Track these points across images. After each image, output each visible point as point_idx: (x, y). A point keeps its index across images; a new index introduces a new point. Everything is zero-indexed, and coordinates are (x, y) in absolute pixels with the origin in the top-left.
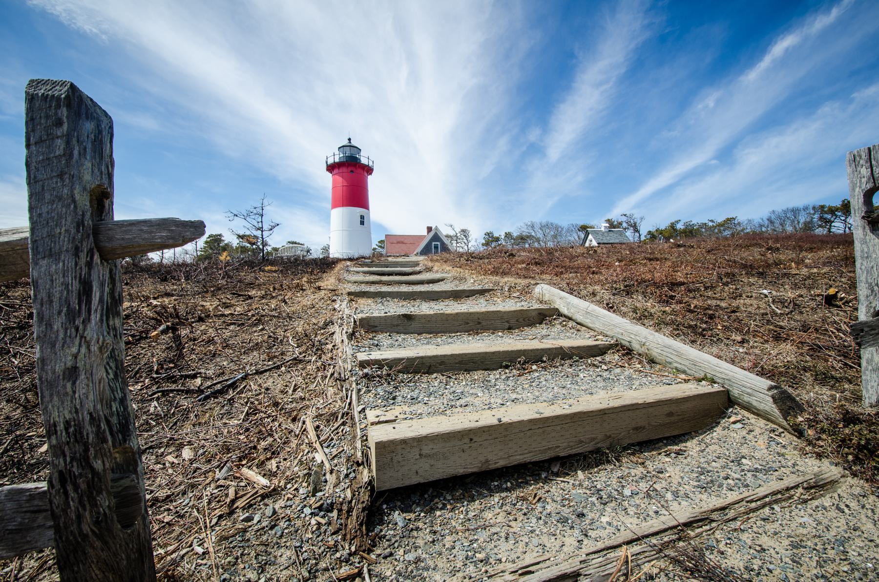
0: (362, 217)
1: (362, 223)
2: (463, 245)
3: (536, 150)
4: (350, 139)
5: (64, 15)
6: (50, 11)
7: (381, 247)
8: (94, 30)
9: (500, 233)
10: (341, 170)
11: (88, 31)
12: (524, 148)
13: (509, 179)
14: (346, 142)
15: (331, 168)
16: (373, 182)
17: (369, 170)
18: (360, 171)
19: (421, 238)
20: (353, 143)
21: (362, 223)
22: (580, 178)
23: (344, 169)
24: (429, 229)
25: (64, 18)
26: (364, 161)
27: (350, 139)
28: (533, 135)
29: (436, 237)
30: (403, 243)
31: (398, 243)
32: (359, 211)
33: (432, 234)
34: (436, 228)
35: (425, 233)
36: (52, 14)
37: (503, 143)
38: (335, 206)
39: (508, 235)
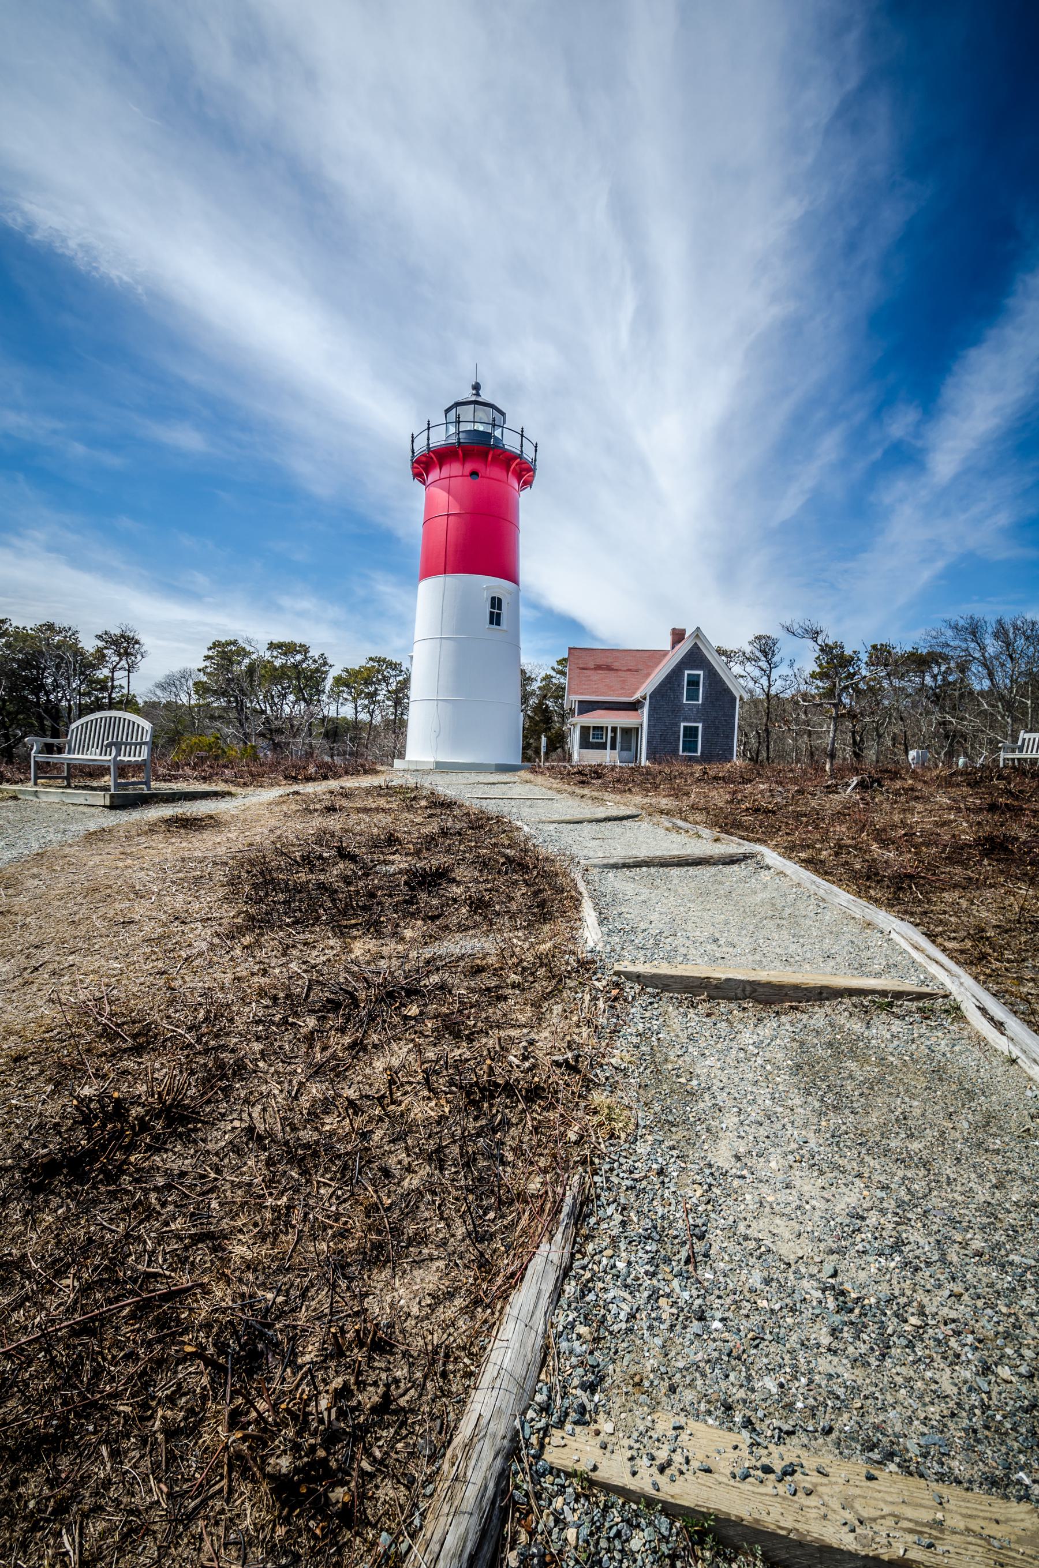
0: (496, 603)
1: (495, 619)
2: (757, 673)
3: (906, 457)
4: (477, 387)
5: (80, 255)
6: (60, 251)
7: (562, 673)
8: (126, 278)
9: (856, 638)
10: (446, 471)
11: (116, 281)
12: (877, 454)
13: (841, 526)
14: (468, 394)
15: (425, 464)
16: (533, 513)
17: (523, 471)
18: (496, 472)
19: (656, 656)
20: (485, 396)
21: (495, 619)
22: (1003, 518)
23: (455, 469)
24: (678, 636)
25: (81, 262)
26: (511, 442)
27: (477, 387)
28: (900, 424)
29: (695, 658)
30: (609, 668)
31: (598, 667)
32: (488, 585)
33: (684, 648)
34: (698, 633)
35: (666, 644)
36: (63, 255)
37: (830, 446)
38: (428, 572)
39: (880, 654)
